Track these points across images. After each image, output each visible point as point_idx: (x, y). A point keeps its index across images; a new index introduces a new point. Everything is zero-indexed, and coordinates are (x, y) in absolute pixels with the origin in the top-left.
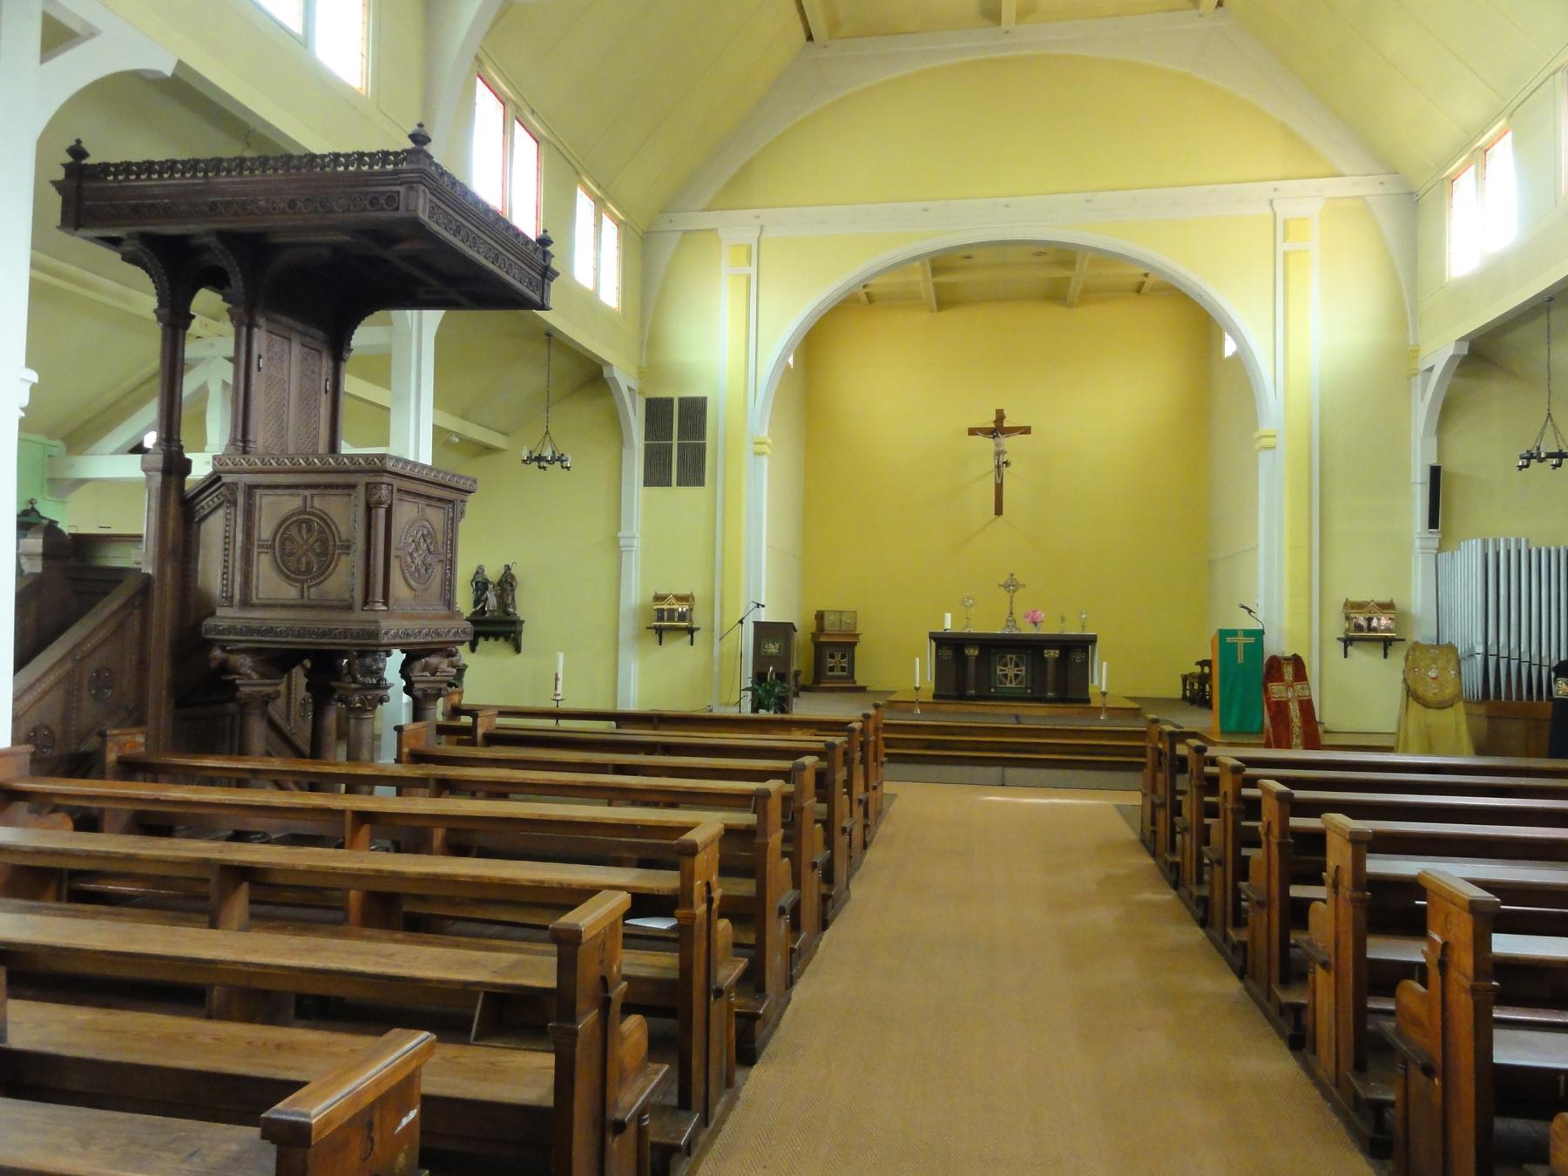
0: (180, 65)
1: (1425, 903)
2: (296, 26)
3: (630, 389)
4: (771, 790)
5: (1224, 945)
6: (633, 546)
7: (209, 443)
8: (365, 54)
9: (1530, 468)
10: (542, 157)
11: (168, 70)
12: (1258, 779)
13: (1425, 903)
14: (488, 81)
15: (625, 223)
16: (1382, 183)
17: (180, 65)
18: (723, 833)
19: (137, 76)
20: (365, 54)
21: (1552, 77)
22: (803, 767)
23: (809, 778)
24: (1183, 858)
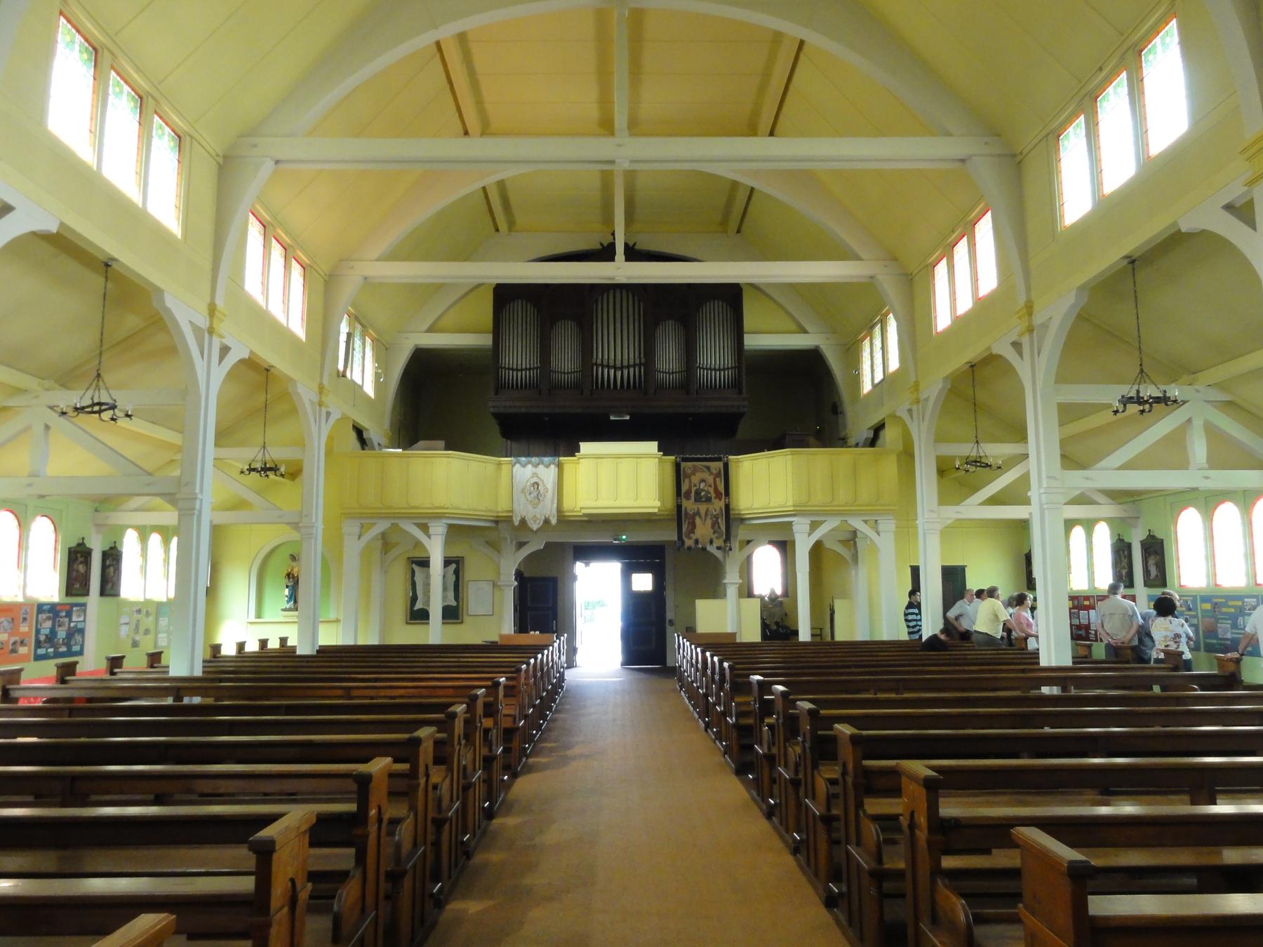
0: (62, 225)
1: (773, 697)
2: (360, 382)
3: (379, 444)
4: (374, 774)
5: (786, 835)
6: (194, 509)
7: (729, 629)
8: (93, 130)
9: (1152, 412)
10: (307, 287)
11: (54, 229)
12: (1013, 826)
13: (773, 697)
14: (167, 120)
15: (378, 340)
16: (885, 266)
17: (62, 225)
18: (314, 821)
19: (34, 233)
20: (138, 171)
21: (1045, 139)
22: (417, 742)
23: (459, 726)
24: (849, 887)
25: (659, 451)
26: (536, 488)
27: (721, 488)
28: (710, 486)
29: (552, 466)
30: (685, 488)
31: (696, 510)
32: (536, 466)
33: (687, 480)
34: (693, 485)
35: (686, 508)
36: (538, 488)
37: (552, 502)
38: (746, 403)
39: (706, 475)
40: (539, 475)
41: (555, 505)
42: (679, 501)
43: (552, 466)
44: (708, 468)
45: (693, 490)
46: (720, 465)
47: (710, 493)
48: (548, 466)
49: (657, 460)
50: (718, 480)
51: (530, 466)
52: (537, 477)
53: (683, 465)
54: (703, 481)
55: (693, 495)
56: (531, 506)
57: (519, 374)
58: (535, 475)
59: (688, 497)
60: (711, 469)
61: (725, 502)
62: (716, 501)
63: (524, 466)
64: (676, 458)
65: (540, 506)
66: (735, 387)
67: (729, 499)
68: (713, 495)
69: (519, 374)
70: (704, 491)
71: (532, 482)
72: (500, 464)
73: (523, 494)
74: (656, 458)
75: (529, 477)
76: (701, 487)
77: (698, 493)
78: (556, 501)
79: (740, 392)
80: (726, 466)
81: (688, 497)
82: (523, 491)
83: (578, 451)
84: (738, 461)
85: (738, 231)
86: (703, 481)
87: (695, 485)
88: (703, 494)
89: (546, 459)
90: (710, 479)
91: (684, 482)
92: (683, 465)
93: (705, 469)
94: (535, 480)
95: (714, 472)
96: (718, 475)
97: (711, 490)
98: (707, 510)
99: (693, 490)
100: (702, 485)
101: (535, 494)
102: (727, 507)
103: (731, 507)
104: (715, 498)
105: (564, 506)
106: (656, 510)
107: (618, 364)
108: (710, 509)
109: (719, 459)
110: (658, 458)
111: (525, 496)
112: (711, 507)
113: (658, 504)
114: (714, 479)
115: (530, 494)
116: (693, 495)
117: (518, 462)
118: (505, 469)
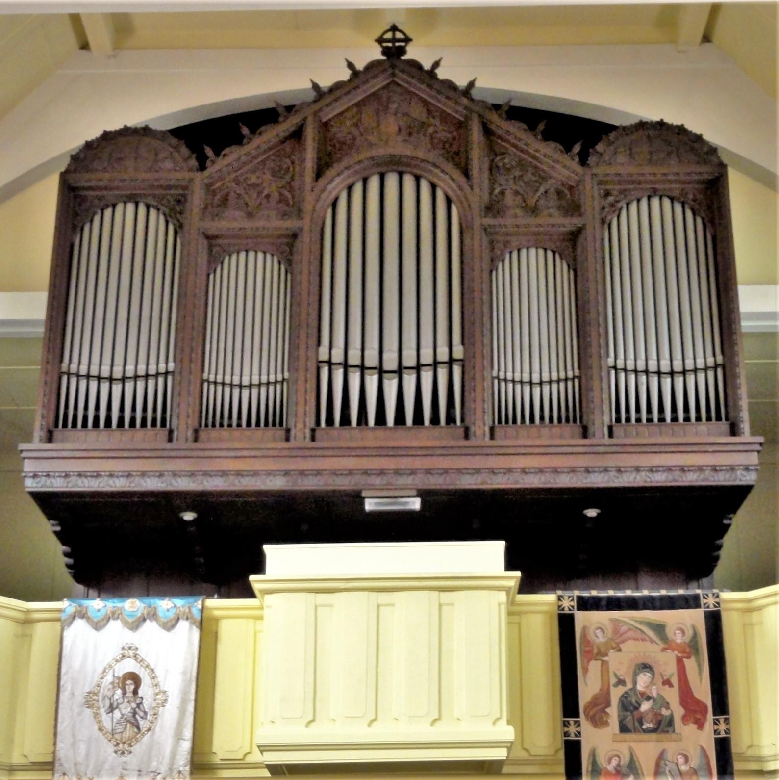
25: (510, 565)
26: (129, 694)
27: (703, 691)
28: (667, 683)
29: (183, 625)
30: (587, 690)
31: (625, 760)
32: (135, 624)
33: (594, 666)
34: (613, 680)
35: (593, 754)
36: (135, 692)
37: (178, 737)
38: (754, 459)
39: (653, 651)
40: (142, 653)
41: (186, 745)
42: (572, 729)
43: (183, 625)
44: (659, 629)
45: (616, 694)
46: (694, 618)
47: (667, 705)
48: (169, 626)
49: (502, 596)
50: (690, 664)
51: (115, 626)
52: (135, 657)
53: (582, 618)
54: (646, 667)
55: (613, 711)
56: (110, 748)
57: (117, 389)
58: (130, 651)
59: (599, 721)
60: (669, 632)
61: (716, 732)
62: (686, 731)
63: (98, 626)
64: (560, 598)
65: (137, 748)
66: (718, 418)
67: (727, 721)
68: (678, 712)
69: (117, 389)
70: (648, 698)
71: (120, 673)
72: (27, 621)
73: (88, 712)
74: (499, 589)
75: (109, 659)
76: (640, 687)
77: (628, 706)
78: (188, 733)
79: (734, 430)
80: (714, 621)
81: (599, 721)
82: (90, 701)
83: (259, 567)
84: (750, 609)
85: (707, 38)
86: (646, 667)
87: (621, 682)
88: (645, 706)
89: (166, 605)
90: (667, 663)
91: (586, 670)
92: (582, 618)
93: (651, 634)
94: (129, 666)
95: (679, 639)
96: (693, 647)
97: (672, 696)
98: (661, 757)
99: (616, 694)
100: (643, 680)
101: (126, 709)
102: (723, 747)
103: (734, 749)
104: (685, 719)
105: (215, 749)
106: (500, 754)
107: (390, 363)
108: (669, 756)
109: (692, 602)
110: (507, 747)
111: (96, 715)
112: (671, 747)
113: (508, 733)
114: (680, 662)
115: (111, 709)
116: (613, 711)
117: (82, 614)
118: (42, 633)
